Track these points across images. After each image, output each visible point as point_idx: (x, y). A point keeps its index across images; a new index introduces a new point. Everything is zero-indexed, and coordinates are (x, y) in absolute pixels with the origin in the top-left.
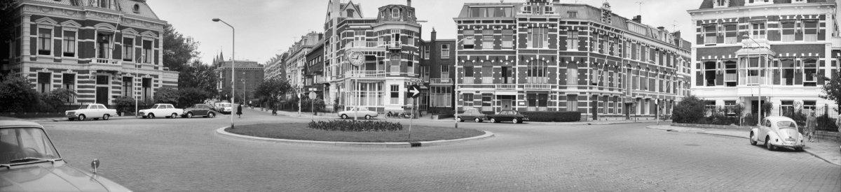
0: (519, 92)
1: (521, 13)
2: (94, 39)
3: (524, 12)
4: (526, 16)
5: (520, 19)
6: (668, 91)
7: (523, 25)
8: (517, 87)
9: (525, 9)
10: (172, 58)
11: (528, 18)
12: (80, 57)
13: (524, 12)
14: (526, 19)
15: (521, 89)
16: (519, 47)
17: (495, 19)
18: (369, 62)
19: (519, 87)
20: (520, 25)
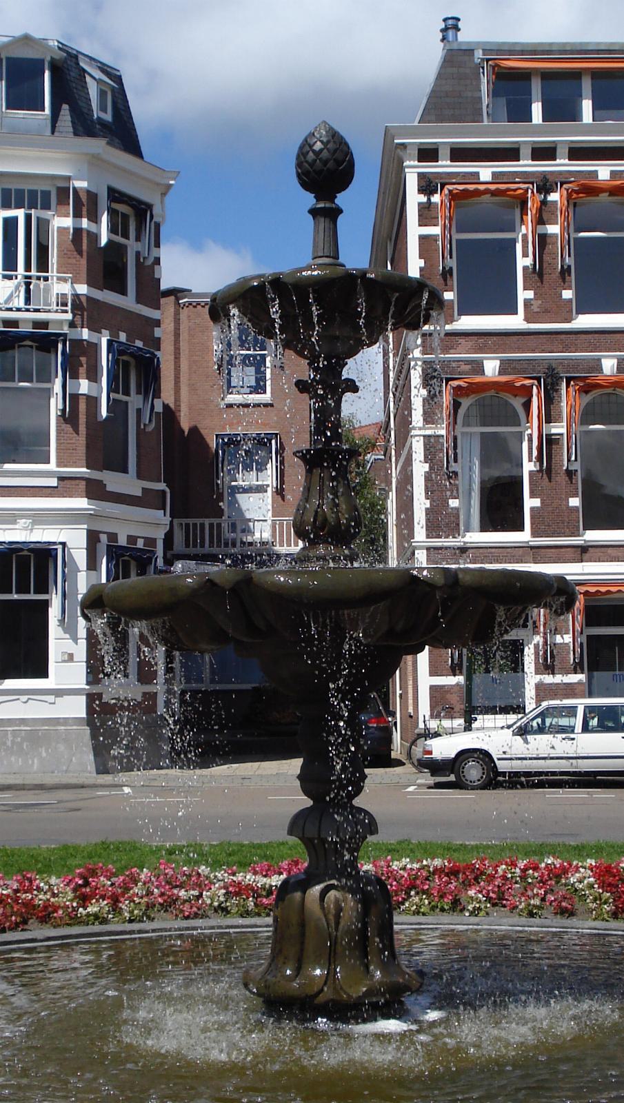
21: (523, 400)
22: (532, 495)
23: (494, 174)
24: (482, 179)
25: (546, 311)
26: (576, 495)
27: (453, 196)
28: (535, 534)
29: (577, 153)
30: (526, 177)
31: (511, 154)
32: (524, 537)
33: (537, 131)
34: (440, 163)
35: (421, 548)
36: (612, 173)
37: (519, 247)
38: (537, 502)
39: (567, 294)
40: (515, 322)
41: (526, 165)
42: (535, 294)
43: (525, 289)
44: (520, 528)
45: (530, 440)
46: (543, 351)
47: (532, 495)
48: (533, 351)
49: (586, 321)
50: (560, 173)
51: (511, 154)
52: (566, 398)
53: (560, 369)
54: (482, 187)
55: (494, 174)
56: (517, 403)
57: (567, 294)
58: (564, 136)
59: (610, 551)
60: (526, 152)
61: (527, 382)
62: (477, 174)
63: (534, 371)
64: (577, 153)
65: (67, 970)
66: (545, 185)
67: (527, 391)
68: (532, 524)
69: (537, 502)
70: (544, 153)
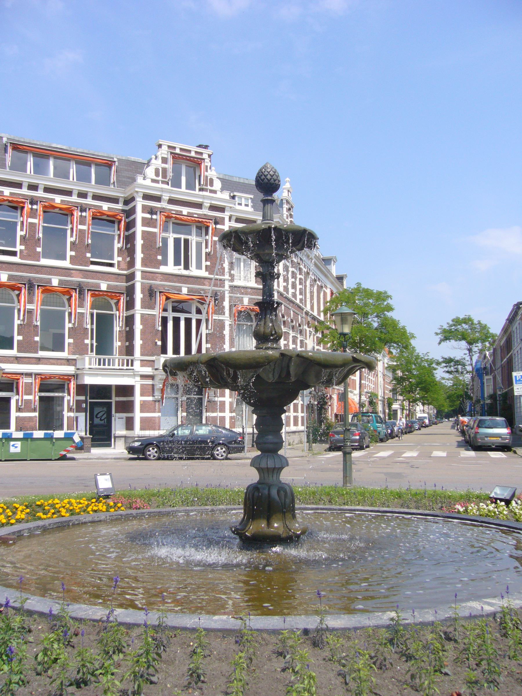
0: (143, 377)
1: (148, 182)
2: (90, 402)
3: (153, 181)
4: (162, 190)
5: (146, 197)
6: (176, 321)
7: (152, 211)
8: (137, 364)
9: (157, 174)
10: (401, 632)
11: (166, 197)
12: (162, 178)
13: (153, 181)
14: (158, 199)
15: (148, 370)
16: (144, 263)
17: (77, 188)
18: (43, 394)
19: (144, 363)
20: (145, 209)
21: (68, 297)
22: (19, 334)
23: (61, 200)
24: (5, 194)
25: (30, 256)
26: (37, 336)
27: (45, 207)
28: (19, 351)
29: (47, 190)
30: (25, 196)
31: (19, 185)
32: (13, 352)
33: (30, 177)
34: (39, 192)
35: (138, 360)
36: (62, 201)
37: (69, 232)
38: (21, 338)
39: (39, 249)
40: (66, 264)
41: (24, 191)
42: (25, 248)
43: (71, 250)
44: (63, 350)
45: (19, 310)
46: (27, 273)
47: (19, 334)
48: (23, 272)
49: (44, 262)
50: (39, 197)
51: (19, 185)
52: (38, 294)
53: (34, 281)
54: (5, 198)
55: (61, 200)
56: (113, 302)
57: (39, 249)
58: (42, 182)
59: (51, 360)
60: (25, 185)
61: (20, 285)
62: (3, 192)
63: (23, 281)
64: (47, 190)
65: (85, 523)
66: (33, 202)
67: (20, 289)
68: (18, 347)
69: (21, 338)
70: (33, 187)
